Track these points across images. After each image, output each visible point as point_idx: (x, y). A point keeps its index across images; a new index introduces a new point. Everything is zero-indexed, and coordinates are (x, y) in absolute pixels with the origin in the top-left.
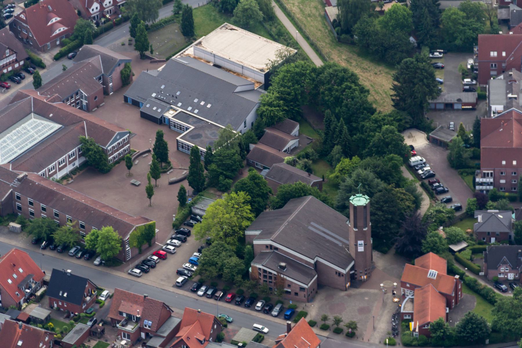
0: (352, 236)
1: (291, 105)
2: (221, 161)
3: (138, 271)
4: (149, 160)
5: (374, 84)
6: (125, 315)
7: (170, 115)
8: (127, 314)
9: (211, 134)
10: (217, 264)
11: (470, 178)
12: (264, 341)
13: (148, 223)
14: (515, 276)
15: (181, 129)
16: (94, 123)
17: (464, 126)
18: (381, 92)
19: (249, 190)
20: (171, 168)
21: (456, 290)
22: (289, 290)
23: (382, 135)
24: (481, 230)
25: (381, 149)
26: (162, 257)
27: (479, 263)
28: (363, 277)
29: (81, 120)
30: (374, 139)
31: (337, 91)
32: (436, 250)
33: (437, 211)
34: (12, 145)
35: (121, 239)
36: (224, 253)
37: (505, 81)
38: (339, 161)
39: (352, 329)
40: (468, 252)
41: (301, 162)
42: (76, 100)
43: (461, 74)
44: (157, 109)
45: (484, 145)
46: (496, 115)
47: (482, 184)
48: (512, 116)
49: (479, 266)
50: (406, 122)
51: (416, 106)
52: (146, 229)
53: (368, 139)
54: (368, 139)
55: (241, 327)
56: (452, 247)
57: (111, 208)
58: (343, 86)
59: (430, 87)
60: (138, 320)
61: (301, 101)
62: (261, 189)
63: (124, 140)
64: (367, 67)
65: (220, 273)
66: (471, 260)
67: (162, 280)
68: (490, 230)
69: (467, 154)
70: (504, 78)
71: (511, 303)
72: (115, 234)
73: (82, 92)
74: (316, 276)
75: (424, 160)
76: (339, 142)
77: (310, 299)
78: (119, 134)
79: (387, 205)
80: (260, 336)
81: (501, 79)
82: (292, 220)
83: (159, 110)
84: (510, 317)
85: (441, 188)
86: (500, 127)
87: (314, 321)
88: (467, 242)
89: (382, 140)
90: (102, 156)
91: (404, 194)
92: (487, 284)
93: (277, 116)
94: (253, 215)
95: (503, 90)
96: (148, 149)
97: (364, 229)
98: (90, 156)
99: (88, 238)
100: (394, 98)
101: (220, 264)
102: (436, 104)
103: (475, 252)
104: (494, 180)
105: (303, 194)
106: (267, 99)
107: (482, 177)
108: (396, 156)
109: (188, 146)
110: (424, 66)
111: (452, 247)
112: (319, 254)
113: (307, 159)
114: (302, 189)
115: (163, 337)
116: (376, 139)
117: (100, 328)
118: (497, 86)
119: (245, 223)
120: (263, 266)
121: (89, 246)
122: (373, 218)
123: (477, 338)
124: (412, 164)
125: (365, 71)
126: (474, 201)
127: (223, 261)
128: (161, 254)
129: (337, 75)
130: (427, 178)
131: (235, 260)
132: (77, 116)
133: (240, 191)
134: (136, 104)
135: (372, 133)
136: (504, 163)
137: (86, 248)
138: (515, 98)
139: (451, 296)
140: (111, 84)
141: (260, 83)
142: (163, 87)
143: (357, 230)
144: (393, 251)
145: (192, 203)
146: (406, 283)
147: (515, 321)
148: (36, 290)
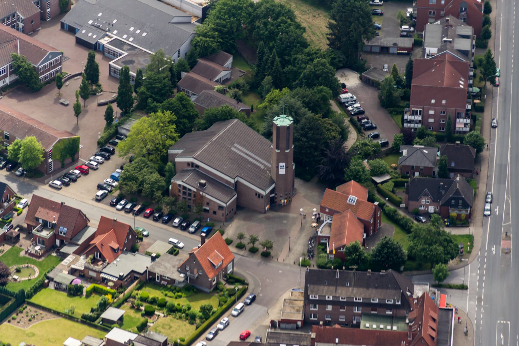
0: (274, 158)
1: (226, 38)
2: (151, 84)
4: (78, 82)
5: (312, 25)
6: (41, 221)
7: (105, 41)
8: (43, 221)
9: (144, 61)
10: (138, 179)
11: (400, 117)
12: (179, 255)
13: (72, 137)
14: (435, 209)
15: (114, 55)
16: (27, 42)
17: (397, 67)
18: (318, 33)
19: (175, 110)
20: (102, 91)
22: (208, 208)
24: (406, 163)
25: (312, 81)
26: (84, 173)
29: (15, 38)
30: (305, 71)
31: (272, 25)
32: (358, 178)
33: (362, 144)
35: (44, 150)
36: (145, 169)
38: (268, 91)
40: (391, 184)
41: (232, 92)
43: (399, 21)
44: (93, 35)
45: (414, 83)
47: (410, 122)
48: (445, 59)
49: (400, 198)
50: (340, 61)
51: (351, 47)
54: (300, 71)
55: (156, 241)
56: (374, 178)
57: (37, 121)
58: (279, 20)
59: (365, 26)
60: (54, 226)
61: (236, 34)
62: (187, 111)
63: (56, 61)
64: (306, 10)
66: (393, 192)
67: (82, 193)
69: (398, 93)
70: (441, 24)
71: (427, 229)
73: (19, 14)
74: (236, 196)
75: (355, 98)
76: (269, 73)
77: (229, 219)
78: (51, 53)
79: (312, 132)
80: (175, 250)
81: (438, 24)
82: (215, 140)
83: (95, 37)
84: (425, 243)
85: (370, 125)
86: (432, 68)
87: (231, 239)
89: (313, 72)
90: (32, 74)
91: (331, 125)
92: (406, 215)
93: (211, 47)
95: (439, 34)
97: (287, 151)
99: (11, 148)
100: (328, 36)
101: (141, 179)
102: (371, 46)
103: (398, 185)
104: (422, 118)
106: (202, 30)
110: (360, 5)
111: (374, 178)
112: (240, 174)
113: (237, 88)
115: (78, 245)
116: (307, 71)
117: (15, 232)
118: (433, 31)
119: (169, 142)
120: (182, 181)
121: (12, 155)
122: (297, 144)
123: (391, 263)
124: (343, 101)
125: (304, 13)
126: (401, 137)
127: (144, 177)
128: (84, 169)
129: (274, 10)
131: (156, 176)
133: (167, 111)
134: (72, 30)
135: (303, 65)
136: (433, 101)
137: (8, 158)
138: (450, 42)
141: (198, 17)
142: (100, 15)
143: (279, 151)
144: (316, 179)
145: (119, 123)
146: (325, 208)
147: (431, 247)
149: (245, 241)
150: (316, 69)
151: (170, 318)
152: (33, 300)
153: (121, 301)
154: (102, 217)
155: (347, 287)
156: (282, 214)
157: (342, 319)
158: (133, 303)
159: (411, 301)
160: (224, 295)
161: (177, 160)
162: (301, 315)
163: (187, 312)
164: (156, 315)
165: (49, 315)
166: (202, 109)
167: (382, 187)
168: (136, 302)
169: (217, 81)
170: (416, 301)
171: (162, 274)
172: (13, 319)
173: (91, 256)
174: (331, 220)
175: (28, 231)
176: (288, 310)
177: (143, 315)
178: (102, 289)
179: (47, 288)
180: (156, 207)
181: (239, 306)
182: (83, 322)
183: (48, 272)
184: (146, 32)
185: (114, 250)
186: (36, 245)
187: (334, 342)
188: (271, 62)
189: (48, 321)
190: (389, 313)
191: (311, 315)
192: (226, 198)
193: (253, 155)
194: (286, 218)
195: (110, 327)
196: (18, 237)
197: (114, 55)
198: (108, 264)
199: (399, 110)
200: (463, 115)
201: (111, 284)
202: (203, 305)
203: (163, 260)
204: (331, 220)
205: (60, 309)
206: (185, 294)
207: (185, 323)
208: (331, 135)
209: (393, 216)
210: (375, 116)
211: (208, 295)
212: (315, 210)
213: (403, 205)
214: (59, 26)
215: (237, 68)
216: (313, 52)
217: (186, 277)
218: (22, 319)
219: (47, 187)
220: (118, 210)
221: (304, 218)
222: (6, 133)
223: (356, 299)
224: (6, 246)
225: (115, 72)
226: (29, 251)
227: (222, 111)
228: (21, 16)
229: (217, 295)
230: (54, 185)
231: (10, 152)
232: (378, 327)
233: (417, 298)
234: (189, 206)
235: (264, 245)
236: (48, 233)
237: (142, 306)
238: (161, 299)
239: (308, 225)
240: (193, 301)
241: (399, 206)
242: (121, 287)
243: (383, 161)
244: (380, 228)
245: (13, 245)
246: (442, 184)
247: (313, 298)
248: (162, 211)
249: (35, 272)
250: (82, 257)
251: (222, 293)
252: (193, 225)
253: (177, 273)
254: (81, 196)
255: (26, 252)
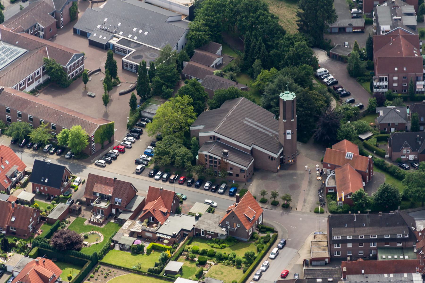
0: (282, 127)
3: (103, 162)
4: (102, 77)
6: (98, 195)
7: (114, 41)
8: (100, 194)
9: (150, 55)
10: (170, 153)
11: (368, 84)
13: (109, 123)
14: (414, 157)
15: (124, 52)
17: (358, 44)
20: (120, 83)
21: (370, 168)
22: (231, 172)
23: (296, 49)
24: (383, 122)
26: (122, 151)
27: (385, 148)
28: (290, 161)
29: (43, 45)
31: (253, 17)
32: (348, 137)
33: (344, 109)
34: (4, 55)
35: (88, 136)
36: (174, 145)
37: (389, 7)
39: (288, 201)
40: (374, 140)
41: (228, 74)
42: (35, 32)
43: (348, 5)
44: (103, 37)
45: (376, 56)
46: (385, 34)
47: (378, 87)
49: (384, 150)
51: (317, 29)
52: (107, 128)
53: (283, 53)
54: (283, 53)
55: (194, 203)
58: (258, 13)
60: (109, 199)
61: (222, 27)
62: (200, 94)
65: (173, 160)
66: (377, 146)
67: (123, 168)
68: (391, 122)
69: (364, 64)
70: (388, 5)
72: (83, 131)
73: (40, 25)
74: (253, 160)
75: (328, 71)
77: (249, 180)
79: (307, 103)
81: (385, 6)
82: (230, 116)
83: (105, 38)
84: (418, 186)
86: (390, 42)
88: (372, 132)
94: (196, 114)
96: (98, 68)
97: (292, 120)
98: (53, 73)
99: (61, 136)
100: (298, 23)
101: (172, 153)
102: (331, 28)
103: (379, 140)
105: (236, 96)
107: (378, 82)
108: (308, 66)
109: (132, 65)
113: (232, 71)
114: (235, 92)
115: (132, 212)
117: (77, 206)
119: (190, 121)
120: (209, 152)
124: (318, 74)
126: (374, 100)
127: (174, 150)
128: (121, 148)
129: (252, 5)
130: (331, 84)
131: (184, 150)
132: (39, 42)
134: (84, 35)
136: (396, 69)
138: (400, 19)
139: (365, 172)
140: (62, 19)
141: (186, 15)
142: (106, 20)
143: (286, 121)
144: (312, 139)
145: (142, 108)
146: (327, 164)
148: (20, 179)
149: (268, 197)
150: (298, 51)
151: (220, 265)
152: (104, 260)
153: (177, 255)
154: (150, 187)
155: (364, 227)
156: (291, 172)
157: (361, 253)
158: (187, 256)
159: (417, 234)
160: (259, 242)
161: (201, 135)
162: (327, 253)
163: (234, 259)
164: (208, 264)
165: (120, 271)
166: (211, 93)
167: (368, 142)
168: (190, 255)
169: (215, 65)
170: (420, 234)
171: (207, 230)
172: (91, 277)
173: (146, 220)
174: (334, 174)
175: (87, 204)
176: (316, 250)
177: (197, 265)
178: (159, 247)
179: (113, 250)
180: (187, 174)
181: (275, 250)
182: (149, 275)
183: (112, 237)
184: (147, 31)
185: (163, 213)
186: (97, 215)
187: (361, 273)
188: (258, 47)
189: (121, 277)
190: (399, 245)
191: (335, 252)
192: (246, 163)
193: (261, 126)
194: (295, 174)
195: (174, 278)
196: (80, 209)
197: (124, 52)
198: (161, 225)
199: (366, 78)
200: (421, 78)
201: (166, 241)
202: (247, 252)
203: (205, 218)
204: (334, 174)
205: (128, 266)
206: (228, 244)
207: (233, 268)
208: (320, 104)
209: (382, 166)
210: (346, 84)
211: (246, 244)
212: (317, 166)
213: (387, 156)
214: (72, 31)
215: (226, 55)
216: (292, 37)
217: (227, 230)
218: (99, 277)
219: (93, 166)
220: (156, 180)
221: (310, 173)
222: (53, 124)
223: (372, 237)
224: (71, 217)
225: (127, 66)
226: (92, 221)
227: (230, 92)
228: (41, 26)
229: (254, 242)
230: (100, 164)
231: (60, 140)
232: (393, 257)
233: (421, 231)
234: (216, 172)
235: (284, 199)
236: (106, 204)
237: (195, 257)
238: (210, 251)
239: (314, 179)
240: (236, 250)
241: (384, 157)
242: (175, 243)
243: (365, 121)
244: (373, 176)
245: (76, 216)
246: (418, 136)
247: (337, 239)
248: (193, 177)
249: (100, 237)
250: (137, 222)
251: (258, 241)
252: (221, 187)
253: (219, 228)
254: (122, 169)
255: (89, 221)
